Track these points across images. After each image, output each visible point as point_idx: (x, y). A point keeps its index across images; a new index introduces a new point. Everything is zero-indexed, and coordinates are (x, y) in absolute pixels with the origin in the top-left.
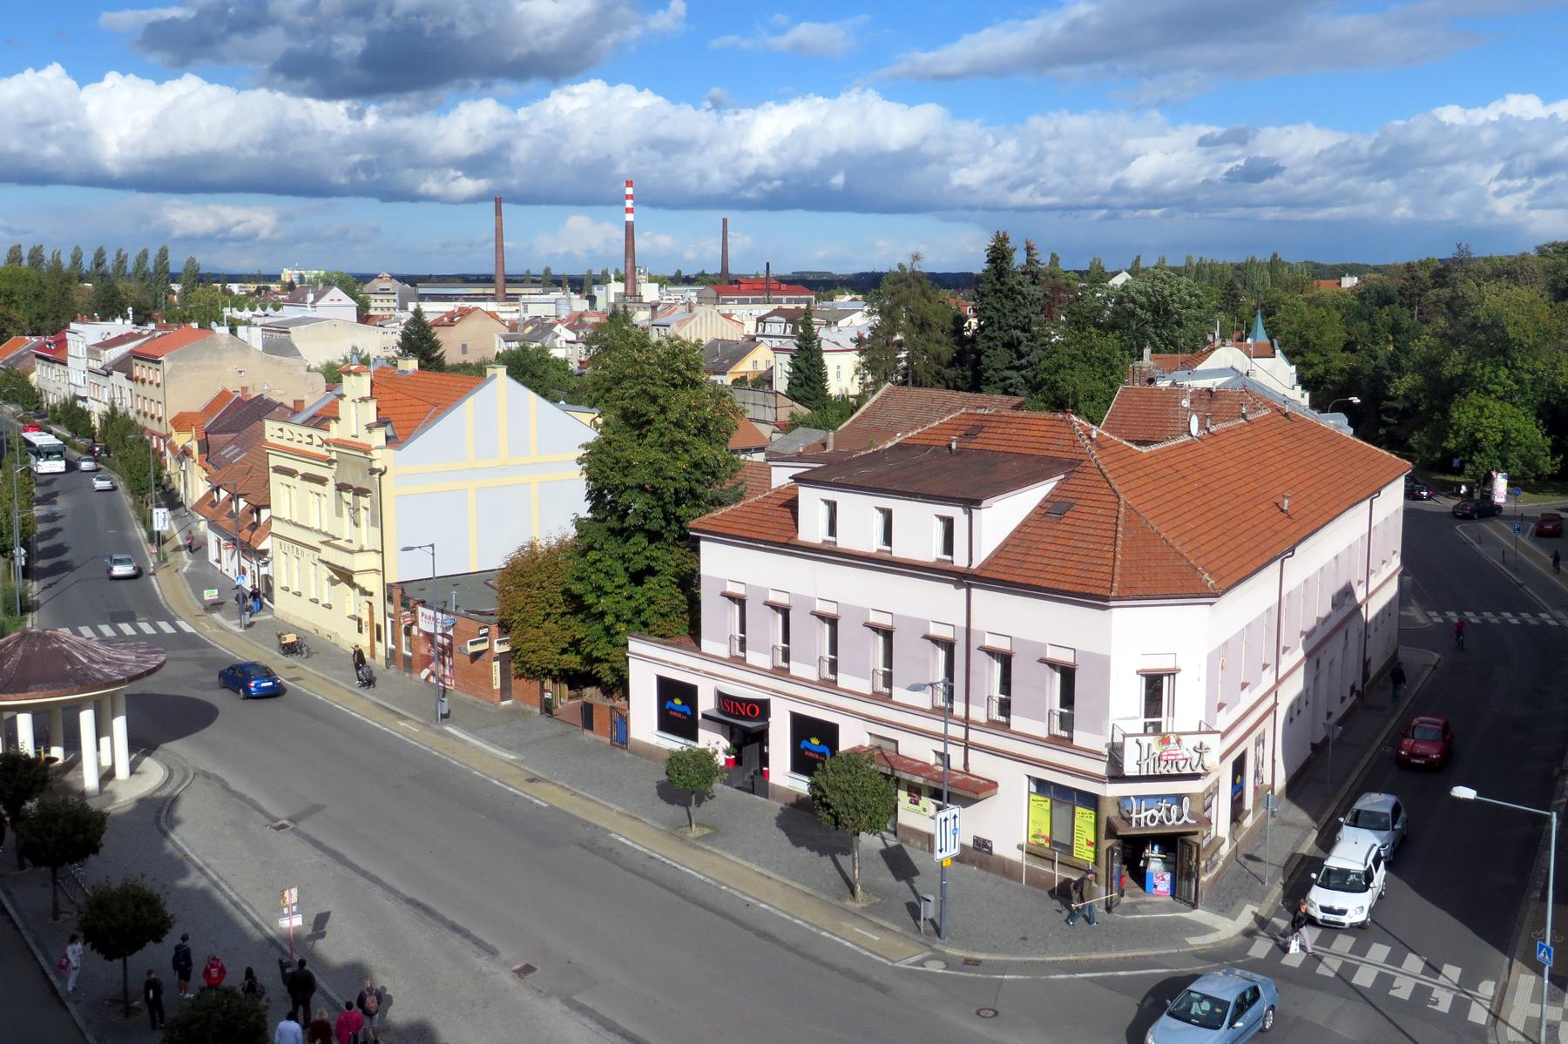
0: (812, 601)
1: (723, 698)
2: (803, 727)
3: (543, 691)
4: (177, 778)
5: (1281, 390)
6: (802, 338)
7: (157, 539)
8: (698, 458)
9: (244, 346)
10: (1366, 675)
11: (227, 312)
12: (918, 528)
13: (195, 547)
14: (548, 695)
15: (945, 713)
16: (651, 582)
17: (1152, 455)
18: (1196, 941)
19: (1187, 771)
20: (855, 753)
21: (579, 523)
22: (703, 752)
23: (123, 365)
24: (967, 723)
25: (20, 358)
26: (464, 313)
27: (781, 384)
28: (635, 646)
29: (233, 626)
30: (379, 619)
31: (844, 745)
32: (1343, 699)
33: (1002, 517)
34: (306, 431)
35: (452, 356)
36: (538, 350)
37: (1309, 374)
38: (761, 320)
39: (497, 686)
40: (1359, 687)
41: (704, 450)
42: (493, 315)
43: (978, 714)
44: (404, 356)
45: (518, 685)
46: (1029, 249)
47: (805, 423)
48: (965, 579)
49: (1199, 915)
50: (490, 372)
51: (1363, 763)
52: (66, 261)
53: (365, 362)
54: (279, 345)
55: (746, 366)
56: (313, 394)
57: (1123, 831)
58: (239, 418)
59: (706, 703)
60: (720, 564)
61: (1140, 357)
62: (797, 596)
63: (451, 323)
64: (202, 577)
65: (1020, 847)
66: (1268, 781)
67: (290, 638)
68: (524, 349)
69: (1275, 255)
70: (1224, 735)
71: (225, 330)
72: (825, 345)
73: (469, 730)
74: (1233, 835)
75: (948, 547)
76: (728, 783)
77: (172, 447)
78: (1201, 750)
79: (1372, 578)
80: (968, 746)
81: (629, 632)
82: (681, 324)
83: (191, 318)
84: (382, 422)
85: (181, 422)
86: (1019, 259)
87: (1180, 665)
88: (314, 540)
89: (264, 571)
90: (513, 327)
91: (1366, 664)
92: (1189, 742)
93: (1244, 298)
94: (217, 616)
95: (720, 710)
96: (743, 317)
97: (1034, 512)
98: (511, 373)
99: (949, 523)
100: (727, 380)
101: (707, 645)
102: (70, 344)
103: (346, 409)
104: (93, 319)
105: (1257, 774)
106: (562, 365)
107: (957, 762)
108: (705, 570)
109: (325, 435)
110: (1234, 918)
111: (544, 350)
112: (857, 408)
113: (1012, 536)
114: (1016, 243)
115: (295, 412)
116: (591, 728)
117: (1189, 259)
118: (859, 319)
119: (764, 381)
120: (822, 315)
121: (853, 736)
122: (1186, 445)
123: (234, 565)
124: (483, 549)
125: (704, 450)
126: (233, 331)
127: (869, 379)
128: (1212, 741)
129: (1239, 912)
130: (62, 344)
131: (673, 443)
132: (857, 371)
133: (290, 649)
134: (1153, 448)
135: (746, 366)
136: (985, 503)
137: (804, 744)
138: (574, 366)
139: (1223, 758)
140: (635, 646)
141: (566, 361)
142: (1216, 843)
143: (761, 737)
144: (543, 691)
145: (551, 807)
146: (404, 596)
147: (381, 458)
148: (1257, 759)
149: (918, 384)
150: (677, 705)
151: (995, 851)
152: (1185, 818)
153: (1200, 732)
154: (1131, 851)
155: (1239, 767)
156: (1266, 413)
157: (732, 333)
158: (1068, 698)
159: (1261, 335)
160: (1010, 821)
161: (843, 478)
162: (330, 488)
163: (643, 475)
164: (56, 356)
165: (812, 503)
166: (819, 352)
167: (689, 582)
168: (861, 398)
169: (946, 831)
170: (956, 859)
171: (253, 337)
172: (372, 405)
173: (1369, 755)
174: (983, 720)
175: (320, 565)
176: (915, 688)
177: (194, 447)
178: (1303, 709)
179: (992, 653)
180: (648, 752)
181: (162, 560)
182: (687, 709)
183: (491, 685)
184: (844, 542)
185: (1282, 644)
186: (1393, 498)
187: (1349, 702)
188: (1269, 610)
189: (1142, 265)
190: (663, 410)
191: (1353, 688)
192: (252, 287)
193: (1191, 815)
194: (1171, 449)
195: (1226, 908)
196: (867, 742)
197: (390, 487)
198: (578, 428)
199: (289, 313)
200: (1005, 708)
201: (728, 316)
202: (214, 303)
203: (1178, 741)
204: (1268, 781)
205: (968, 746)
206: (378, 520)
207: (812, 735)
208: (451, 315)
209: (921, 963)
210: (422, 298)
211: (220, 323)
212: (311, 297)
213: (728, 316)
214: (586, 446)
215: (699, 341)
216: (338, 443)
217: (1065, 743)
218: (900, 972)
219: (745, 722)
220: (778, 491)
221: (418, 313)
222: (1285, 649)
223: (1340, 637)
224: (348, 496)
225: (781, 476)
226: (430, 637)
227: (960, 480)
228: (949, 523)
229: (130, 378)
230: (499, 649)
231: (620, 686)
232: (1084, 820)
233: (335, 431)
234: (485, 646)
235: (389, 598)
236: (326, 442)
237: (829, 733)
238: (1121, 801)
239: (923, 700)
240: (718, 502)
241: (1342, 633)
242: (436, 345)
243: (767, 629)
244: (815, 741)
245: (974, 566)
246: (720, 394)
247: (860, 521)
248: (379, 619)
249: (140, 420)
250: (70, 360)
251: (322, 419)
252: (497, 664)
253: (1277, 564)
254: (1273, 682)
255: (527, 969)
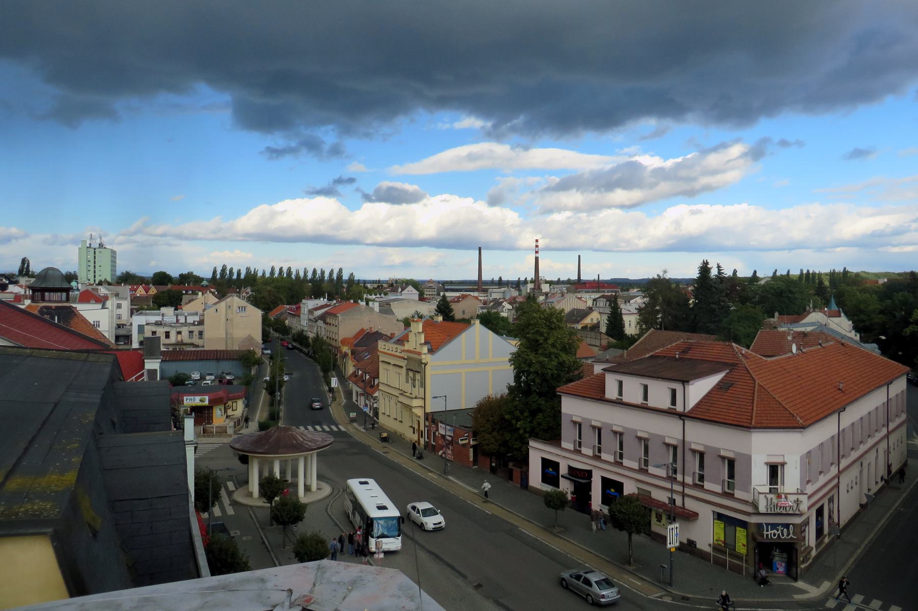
0: (611, 425)
1: (571, 468)
2: (607, 483)
3: (491, 462)
4: (335, 493)
5: (844, 333)
6: (612, 308)
7: (331, 390)
8: (561, 360)
9: (372, 309)
10: (889, 472)
11: (365, 296)
12: (660, 394)
13: (349, 394)
14: (494, 464)
15: (673, 480)
16: (540, 416)
17: (772, 362)
18: (798, 597)
19: (791, 512)
20: (630, 498)
21: (510, 388)
22: (561, 493)
23: (323, 318)
24: (683, 484)
25: (282, 314)
26: (464, 297)
27: (603, 329)
28: (532, 443)
29: (361, 429)
30: (422, 428)
31: (626, 492)
32: (877, 483)
33: (698, 390)
34: (395, 346)
35: (458, 315)
36: (496, 313)
37: (861, 325)
38: (595, 300)
39: (471, 459)
40: (886, 477)
41: (564, 357)
42: (476, 298)
43: (689, 480)
44: (437, 315)
45: (481, 458)
46: (719, 267)
47: (615, 347)
48: (682, 416)
49: (800, 584)
50: (472, 322)
51: (888, 514)
52: (302, 274)
53: (421, 317)
54: (386, 309)
55: (587, 321)
56: (399, 331)
57: (759, 539)
58: (368, 340)
59: (563, 470)
60: (572, 408)
61: (773, 317)
62: (583, 418)
63: (458, 301)
64: (351, 406)
65: (710, 545)
66: (836, 520)
67: (385, 435)
68: (488, 312)
69: (755, 272)
70: (809, 497)
71: (364, 303)
72: (623, 311)
73: (458, 478)
74: (817, 546)
75: (674, 402)
76: (571, 507)
77: (341, 352)
78: (798, 502)
79: (890, 424)
80: (684, 495)
81: (530, 437)
82: (559, 302)
83: (350, 298)
84: (426, 343)
85: (344, 342)
86: (714, 272)
87: (786, 460)
88: (396, 393)
89: (375, 405)
90: (485, 303)
91: (889, 466)
92: (792, 498)
93: (838, 290)
94: (355, 424)
95: (569, 474)
96: (588, 299)
97: (714, 387)
98: (481, 323)
99: (674, 392)
100: (579, 326)
101: (564, 444)
102: (302, 309)
103: (411, 337)
104: (311, 298)
105: (830, 517)
106: (504, 319)
107: (679, 502)
108: (563, 410)
109: (402, 348)
110: (818, 587)
111: (497, 313)
112: (636, 341)
113: (704, 398)
114: (713, 266)
115: (391, 338)
116: (512, 480)
117: (802, 271)
118: (639, 301)
119: (595, 327)
120: (623, 297)
121: (629, 488)
122: (789, 358)
123: (363, 403)
124: (466, 399)
125: (564, 357)
126: (367, 304)
127: (644, 326)
128: (804, 498)
129: (821, 584)
130: (299, 308)
131: (550, 354)
132: (638, 323)
133: (384, 440)
134: (773, 359)
135: (587, 321)
136: (691, 382)
137: (608, 491)
138: (511, 320)
139: (809, 508)
140: (532, 443)
141: (507, 318)
142: (809, 549)
143: (588, 487)
144: (491, 462)
145: (493, 515)
146: (432, 418)
147: (427, 358)
148: (830, 510)
149: (666, 329)
150: (550, 469)
151: (698, 546)
152: (791, 535)
153: (798, 494)
154: (764, 551)
155: (820, 512)
156: (832, 343)
157: (581, 306)
158: (731, 475)
159: (834, 307)
160: (706, 533)
161: (626, 370)
162: (404, 371)
163: (536, 367)
164: (297, 314)
165: (611, 383)
166: (621, 314)
167: (557, 414)
168: (639, 336)
169: (674, 534)
170: (677, 548)
171: (376, 306)
172: (423, 336)
173: (891, 511)
174: (691, 483)
175: (399, 404)
176: (657, 467)
177: (349, 352)
178: (854, 485)
179: (694, 451)
180: (536, 492)
181: (334, 399)
182: (554, 473)
183: (469, 458)
184: (626, 399)
185: (841, 454)
186: (900, 386)
187: (880, 484)
188: (833, 437)
189: (778, 274)
190: (546, 339)
191: (882, 478)
192: (376, 286)
193: (794, 533)
194: (783, 359)
195: (816, 583)
196: (636, 492)
197: (429, 371)
198: (511, 346)
199: (391, 297)
200: (702, 478)
201: (580, 299)
202: (360, 293)
203: (786, 498)
204: (836, 520)
205: (684, 495)
206: (423, 385)
207: (611, 487)
208: (458, 297)
209: (661, 597)
210: (447, 290)
211: (362, 300)
212: (400, 290)
213: (580, 299)
214: (513, 354)
215: (563, 310)
216: (408, 351)
217: (730, 496)
218: (651, 601)
219: (581, 478)
220: (597, 376)
221: (444, 296)
222: (843, 456)
223: (874, 452)
224: (411, 374)
225: (598, 369)
226: (443, 437)
227: (682, 371)
228: (674, 392)
229: (325, 323)
230: (472, 443)
231: (524, 461)
232: (741, 534)
233: (407, 346)
234: (467, 441)
235: (426, 419)
236: (403, 351)
237: (619, 486)
238: (759, 526)
239: (662, 473)
240: (570, 380)
241: (874, 451)
242: (451, 310)
243: (589, 438)
244: (613, 490)
245: (687, 410)
246: (572, 333)
247: (633, 389)
248: (422, 428)
249: (328, 341)
250: (302, 316)
251: (401, 341)
252: (471, 450)
253: (836, 416)
254: (837, 472)
255: (479, 586)
